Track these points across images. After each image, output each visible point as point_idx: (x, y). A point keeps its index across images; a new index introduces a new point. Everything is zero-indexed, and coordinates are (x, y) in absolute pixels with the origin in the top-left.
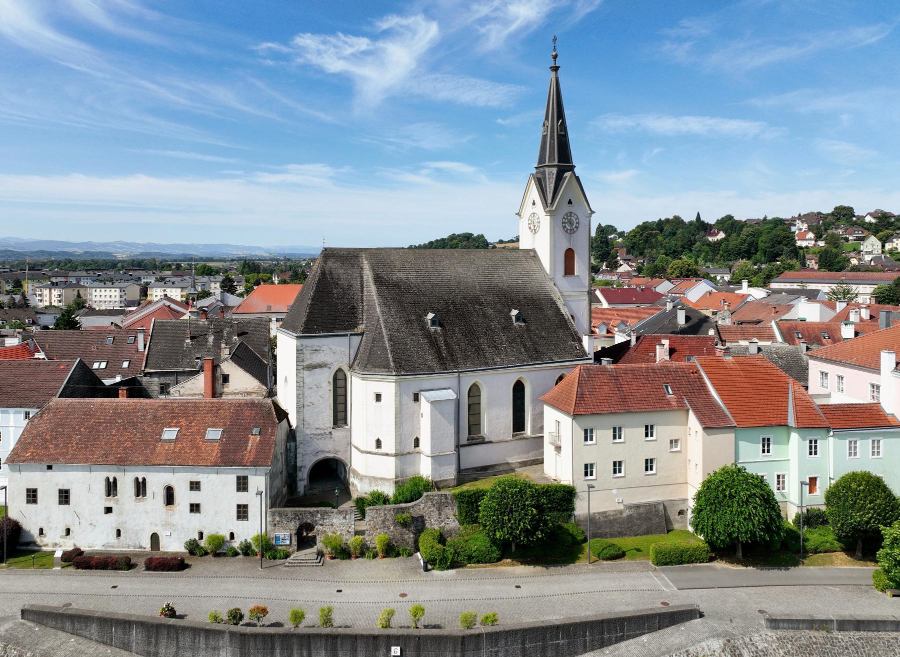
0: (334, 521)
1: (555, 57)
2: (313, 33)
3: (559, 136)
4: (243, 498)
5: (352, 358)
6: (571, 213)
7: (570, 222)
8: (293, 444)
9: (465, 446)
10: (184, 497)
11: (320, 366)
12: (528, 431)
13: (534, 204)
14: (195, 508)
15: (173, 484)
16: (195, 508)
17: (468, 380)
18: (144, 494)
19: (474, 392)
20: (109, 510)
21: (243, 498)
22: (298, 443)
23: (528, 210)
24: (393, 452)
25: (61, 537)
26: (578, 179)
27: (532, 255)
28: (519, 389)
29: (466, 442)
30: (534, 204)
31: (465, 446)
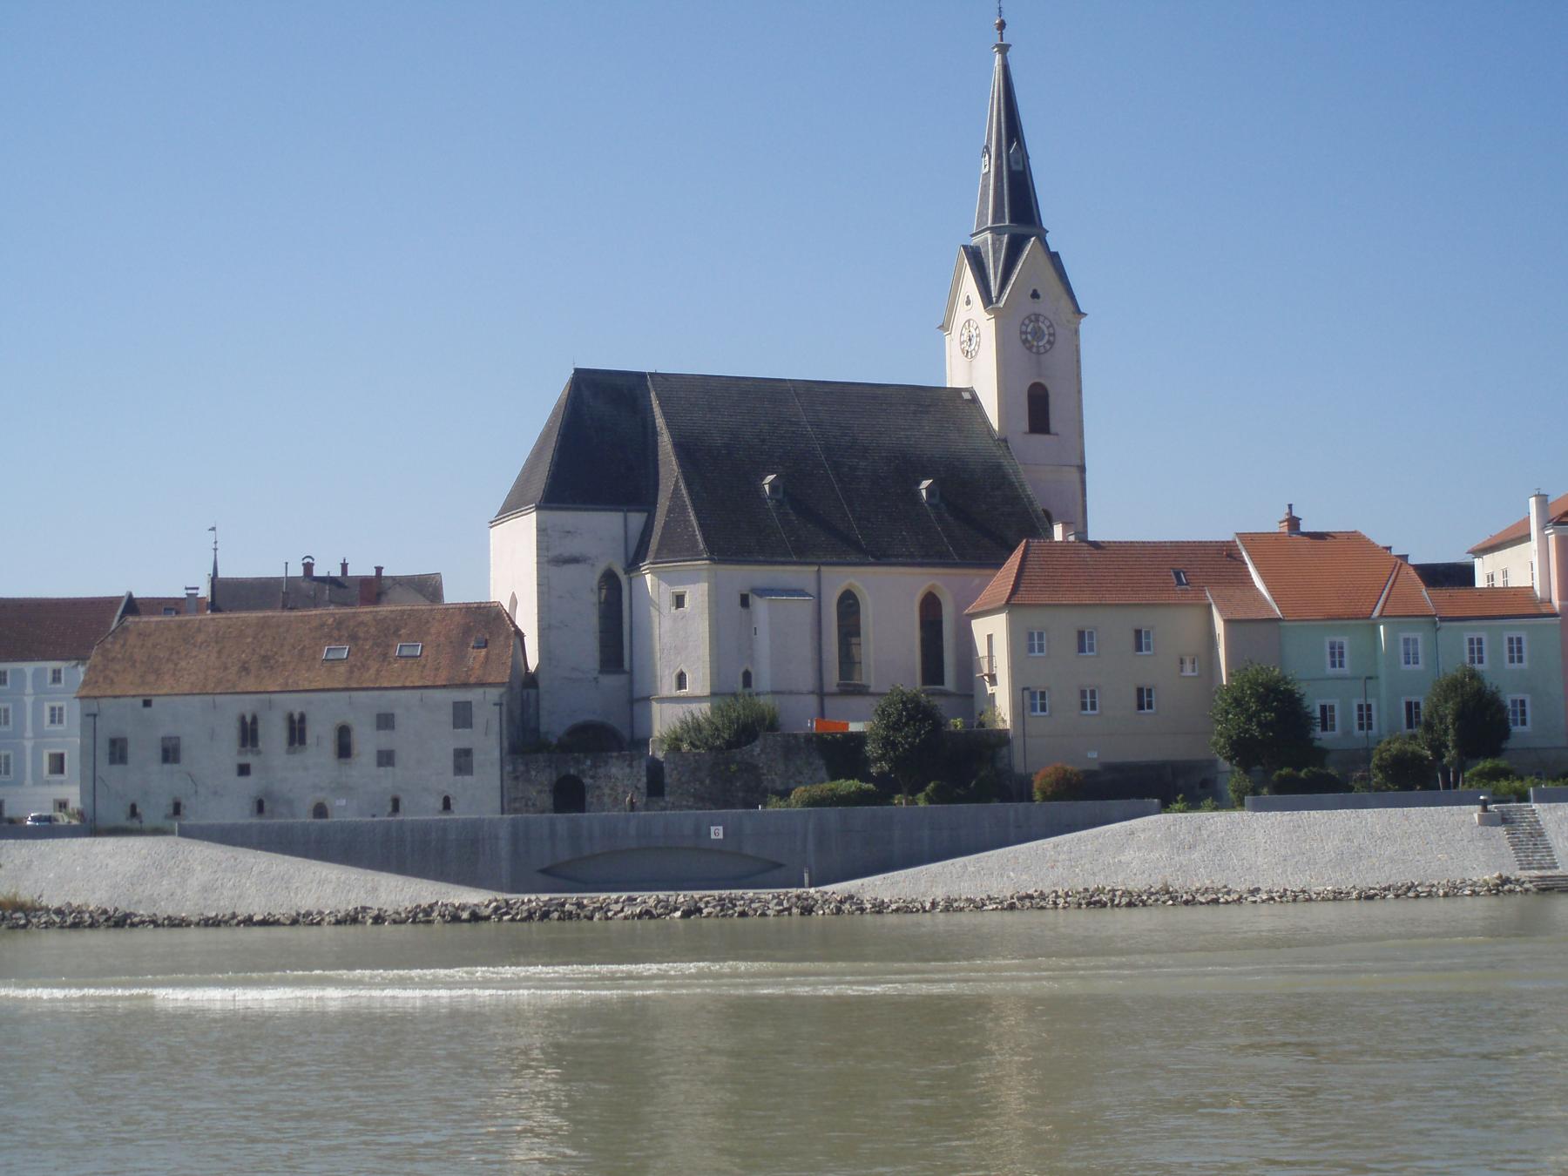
0: (614, 770)
1: (1002, 26)
2: (324, 1014)
3: (1011, 173)
4: (464, 738)
5: (631, 554)
6: (1037, 316)
7: (1038, 334)
8: (532, 692)
9: (832, 694)
10: (366, 742)
11: (574, 560)
12: (950, 683)
13: (968, 302)
14: (386, 758)
15: (350, 719)
16: (386, 758)
17: (839, 578)
18: (302, 741)
19: (849, 605)
20: (244, 770)
21: (464, 738)
22: (541, 690)
23: (961, 314)
24: (707, 692)
25: (167, 817)
26: (1055, 258)
27: (965, 402)
28: (931, 608)
29: (834, 689)
30: (968, 302)
31: (832, 694)
